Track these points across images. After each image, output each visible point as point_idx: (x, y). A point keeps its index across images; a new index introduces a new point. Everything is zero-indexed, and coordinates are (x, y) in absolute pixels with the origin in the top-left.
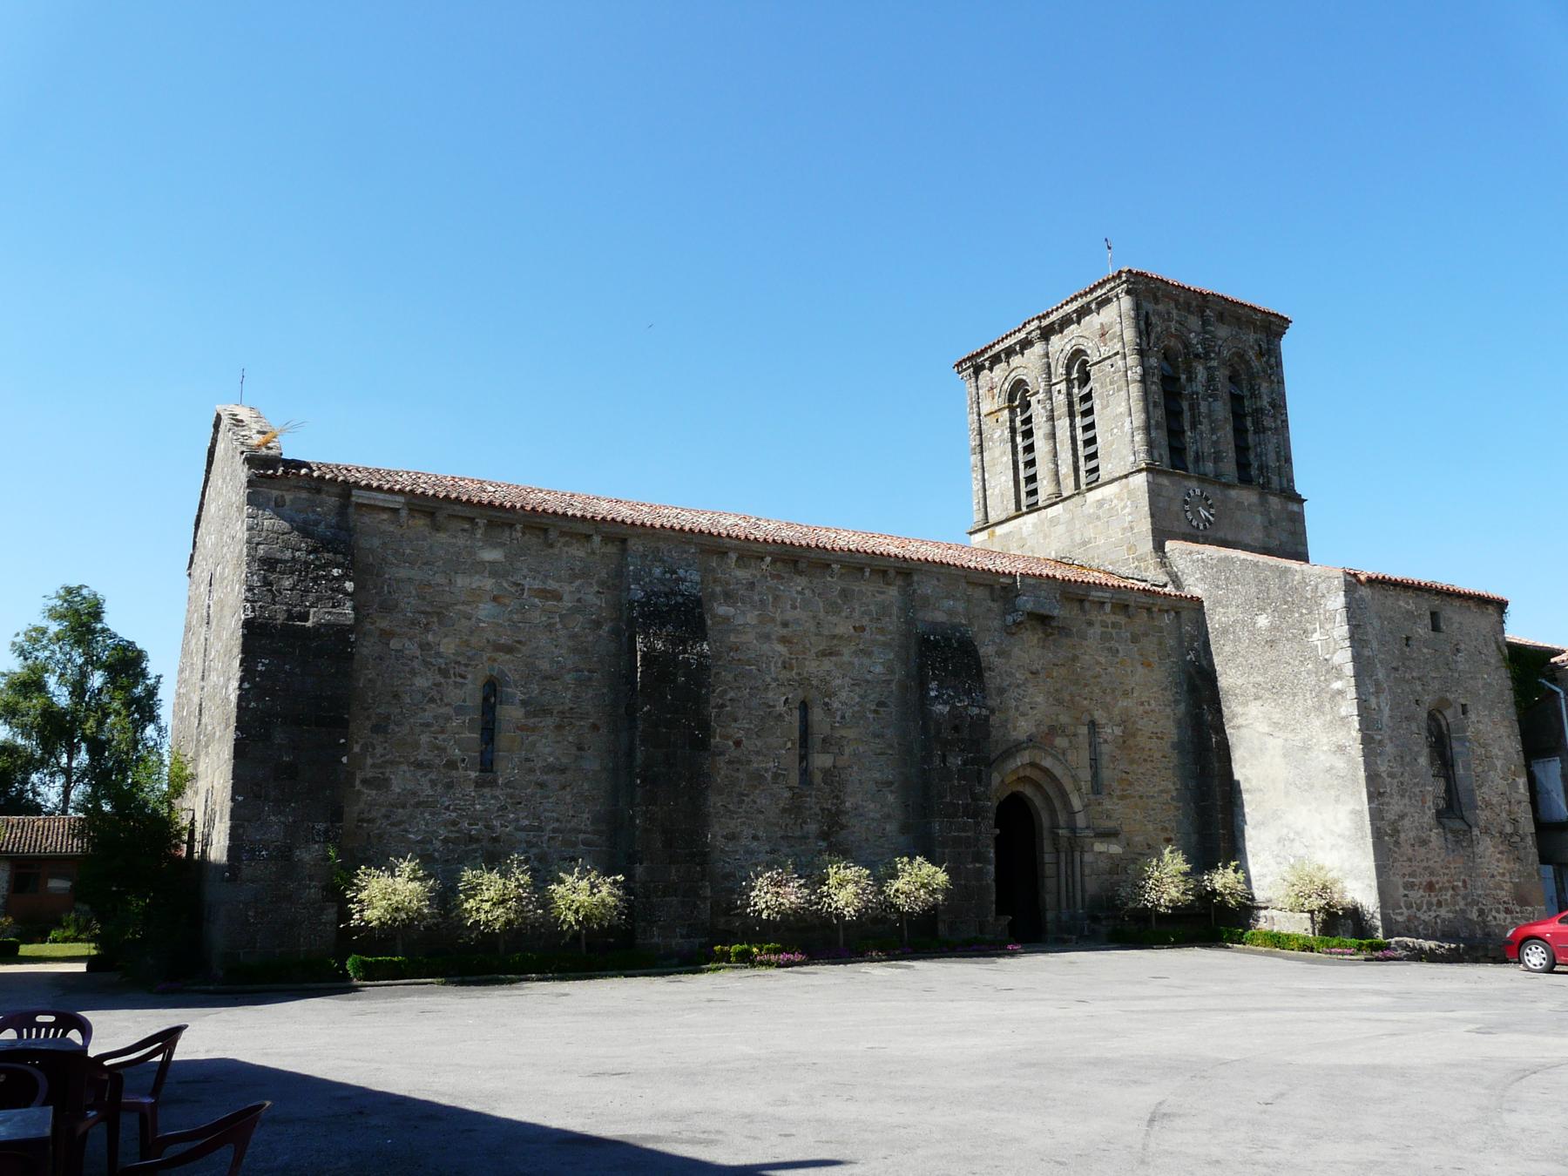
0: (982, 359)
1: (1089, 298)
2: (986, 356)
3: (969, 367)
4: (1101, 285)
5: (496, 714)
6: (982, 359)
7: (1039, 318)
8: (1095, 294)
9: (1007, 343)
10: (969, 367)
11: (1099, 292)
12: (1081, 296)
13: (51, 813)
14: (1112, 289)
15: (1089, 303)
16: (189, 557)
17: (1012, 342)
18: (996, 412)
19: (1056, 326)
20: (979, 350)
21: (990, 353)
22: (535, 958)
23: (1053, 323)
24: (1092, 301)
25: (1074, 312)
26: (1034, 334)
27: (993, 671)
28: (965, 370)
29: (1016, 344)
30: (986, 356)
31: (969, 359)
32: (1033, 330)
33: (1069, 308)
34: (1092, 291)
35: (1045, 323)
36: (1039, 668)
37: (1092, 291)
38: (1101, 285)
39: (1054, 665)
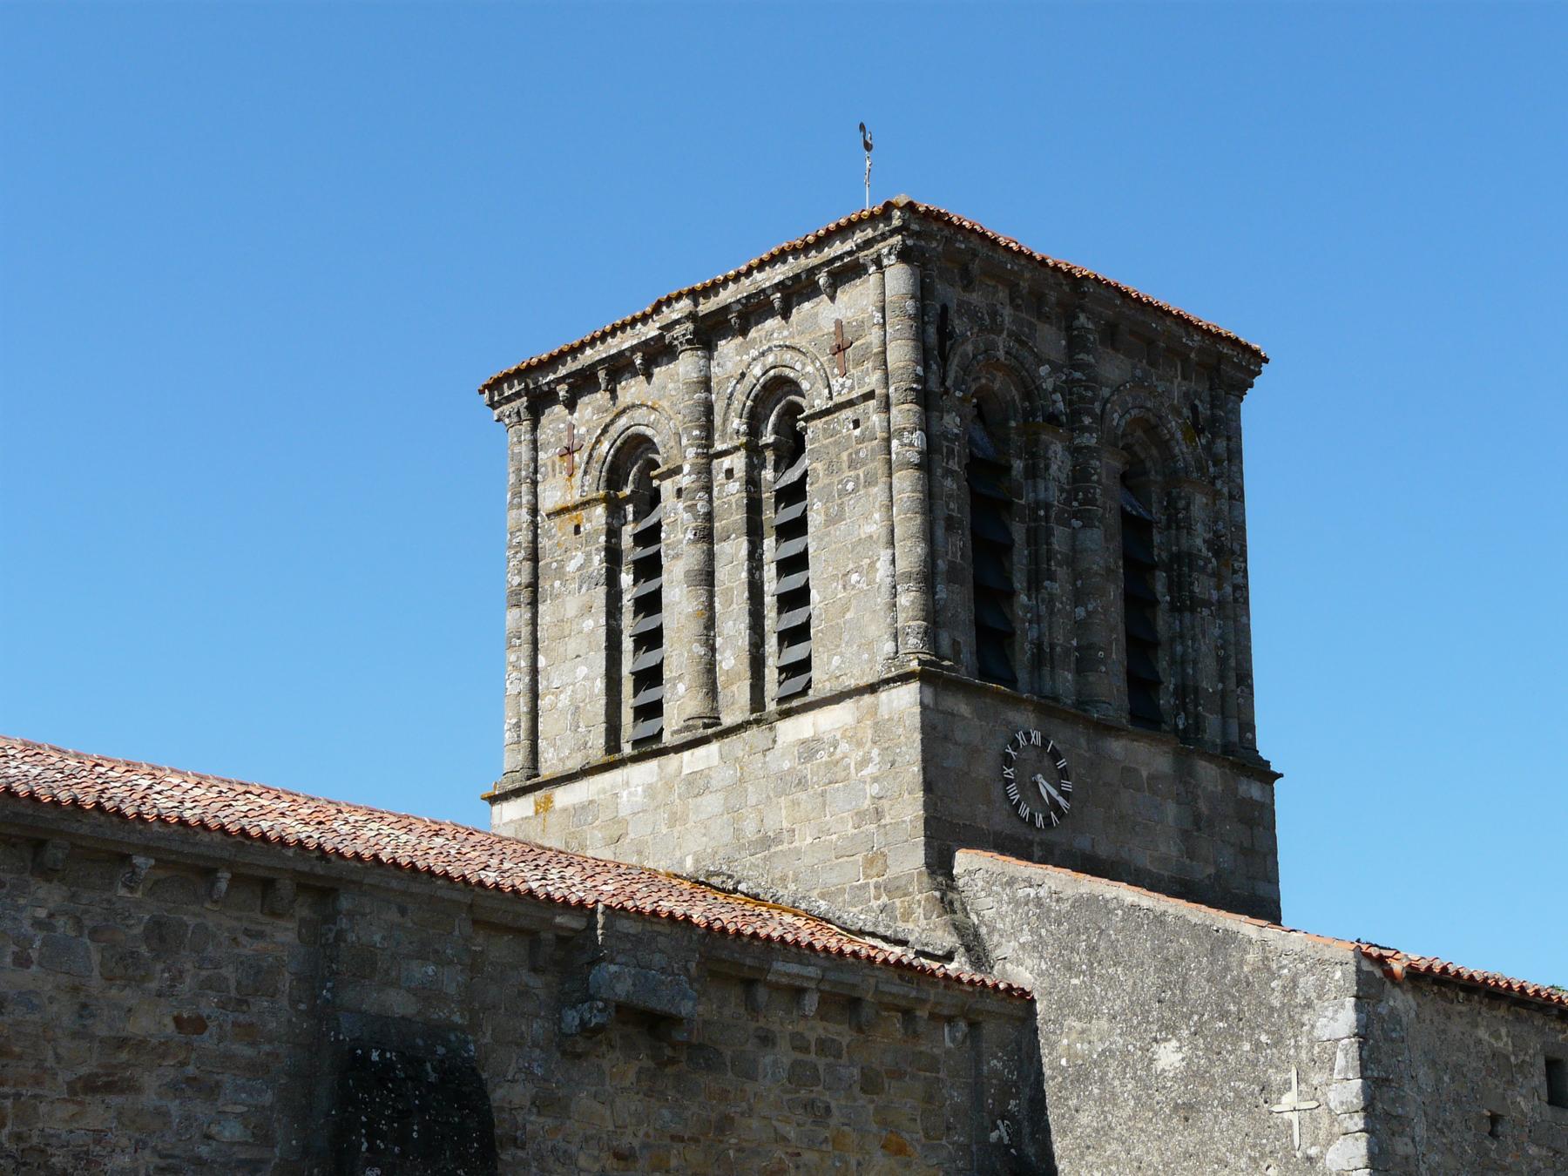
0: (551, 377)
1: (814, 258)
3: (518, 395)
6: (551, 377)
7: (694, 294)
8: (829, 253)
10: (518, 395)
11: (838, 248)
12: (795, 251)
14: (868, 244)
15: (812, 271)
21: (571, 366)
23: (726, 309)
26: (678, 331)
27: (523, 1148)
29: (633, 349)
30: (562, 371)
31: (520, 374)
32: (677, 322)
36: (636, 1144)
39: (673, 1138)
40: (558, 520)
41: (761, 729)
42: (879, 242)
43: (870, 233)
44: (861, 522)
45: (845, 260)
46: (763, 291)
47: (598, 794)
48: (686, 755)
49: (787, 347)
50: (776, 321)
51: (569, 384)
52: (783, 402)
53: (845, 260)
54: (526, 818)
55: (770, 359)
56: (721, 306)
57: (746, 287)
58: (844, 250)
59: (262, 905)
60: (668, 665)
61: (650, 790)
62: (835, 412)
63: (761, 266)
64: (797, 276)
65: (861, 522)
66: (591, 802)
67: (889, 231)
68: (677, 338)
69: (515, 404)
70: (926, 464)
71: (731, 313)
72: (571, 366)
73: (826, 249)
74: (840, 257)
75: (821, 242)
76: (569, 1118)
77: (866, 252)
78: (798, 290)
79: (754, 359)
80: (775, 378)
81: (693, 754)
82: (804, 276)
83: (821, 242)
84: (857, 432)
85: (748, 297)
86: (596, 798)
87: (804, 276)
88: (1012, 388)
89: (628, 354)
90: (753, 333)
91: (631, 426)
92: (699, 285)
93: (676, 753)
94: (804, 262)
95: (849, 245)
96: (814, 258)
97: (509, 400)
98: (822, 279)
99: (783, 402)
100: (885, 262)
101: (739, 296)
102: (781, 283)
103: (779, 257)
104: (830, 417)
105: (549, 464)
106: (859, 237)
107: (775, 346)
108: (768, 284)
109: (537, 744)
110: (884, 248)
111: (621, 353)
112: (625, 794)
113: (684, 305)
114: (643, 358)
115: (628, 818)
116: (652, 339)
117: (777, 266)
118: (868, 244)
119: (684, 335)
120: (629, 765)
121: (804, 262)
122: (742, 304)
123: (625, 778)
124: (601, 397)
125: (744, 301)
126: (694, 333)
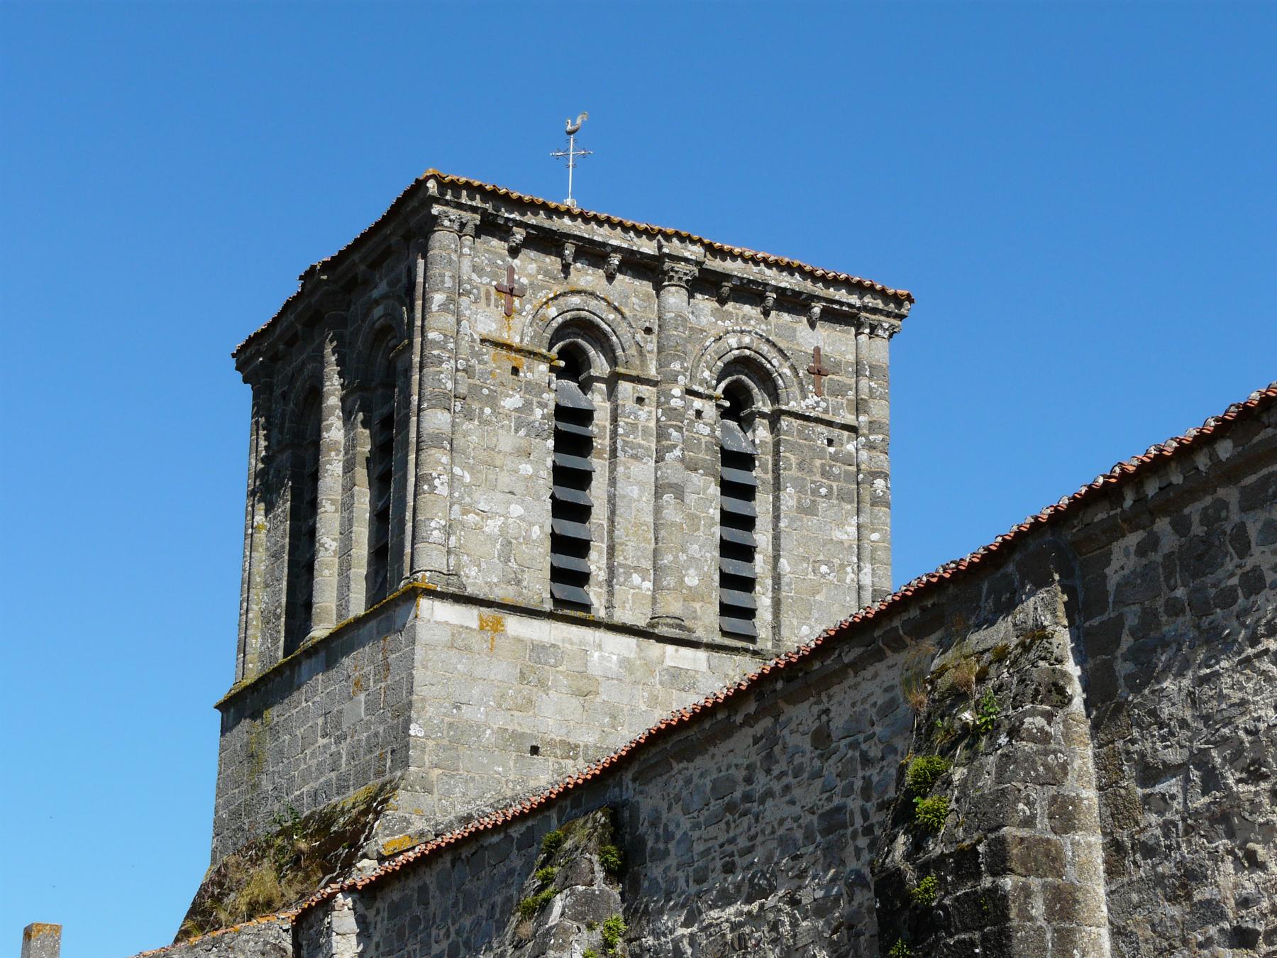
0: (516, 216)
1: (819, 289)
3: (474, 209)
6: (516, 216)
7: (709, 248)
8: (831, 292)
10: (474, 209)
11: (842, 295)
14: (874, 311)
15: (814, 298)
21: (540, 219)
23: (727, 277)
26: (681, 267)
29: (617, 249)
30: (530, 219)
32: (686, 260)
40: (492, 350)
41: (754, 660)
42: (883, 315)
43: (880, 304)
44: (833, 525)
45: (844, 308)
46: (766, 285)
47: (563, 641)
48: (670, 649)
49: (768, 340)
50: (754, 311)
51: (528, 233)
52: (735, 377)
53: (844, 308)
54: (467, 628)
55: (747, 340)
56: (723, 271)
57: (752, 272)
58: (849, 301)
61: (625, 662)
62: (811, 421)
63: (776, 265)
64: (800, 293)
65: (833, 525)
66: (553, 646)
67: (896, 314)
68: (677, 272)
69: (467, 216)
71: (728, 282)
72: (540, 219)
73: (832, 290)
74: (841, 304)
75: (835, 282)
77: (868, 315)
78: (794, 303)
79: (734, 331)
80: (747, 358)
81: (677, 651)
82: (804, 296)
83: (835, 282)
84: (832, 450)
85: (750, 281)
86: (560, 644)
87: (804, 296)
89: (609, 249)
90: (730, 306)
91: (583, 310)
92: (718, 244)
93: (657, 641)
94: (808, 286)
95: (854, 300)
96: (819, 289)
97: (460, 206)
99: (735, 377)
100: (880, 332)
101: (745, 276)
102: (785, 289)
103: (789, 269)
104: (805, 423)
105: (483, 290)
106: (868, 300)
107: (756, 333)
108: (773, 283)
109: (830, 644)
110: (886, 322)
111: (604, 245)
112: (596, 655)
113: (695, 252)
114: (621, 262)
115: (600, 679)
116: (642, 253)
117: (784, 274)
118: (874, 311)
119: (686, 274)
120: (602, 630)
121: (808, 286)
122: (741, 282)
123: (597, 640)
124: (552, 262)
125: (745, 281)
126: (695, 278)
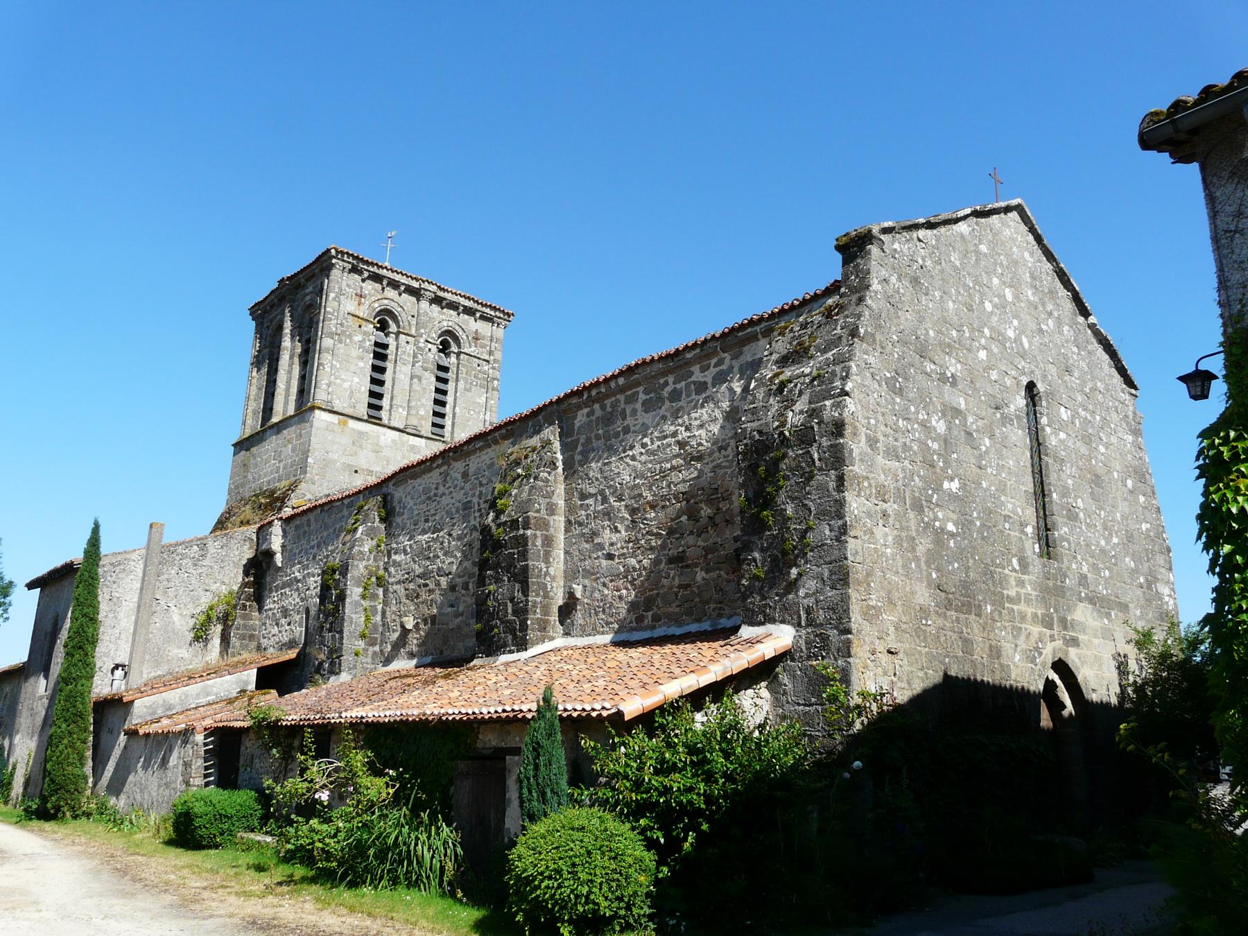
0: (365, 267)
1: (479, 307)
2: (371, 269)
3: (349, 263)
4: (494, 309)
5: (635, 632)
6: (365, 267)
7: (439, 287)
8: (484, 309)
9: (397, 277)
10: (349, 263)
11: (488, 310)
12: (477, 302)
13: (710, 455)
14: (499, 318)
15: (477, 310)
16: (59, 563)
17: (403, 281)
18: (362, 319)
19: (445, 302)
20: (365, 259)
21: (375, 269)
22: (1228, 769)
23: (445, 299)
24: (479, 311)
25: (463, 306)
26: (427, 293)
28: (343, 261)
29: (403, 284)
30: (371, 269)
31: (356, 258)
32: (430, 291)
33: (404, 280)
34: (486, 305)
35: (441, 294)
37: (486, 305)
38: (494, 309)
55: (450, 324)
59: (145, 745)
60: (207, 855)
69: (346, 265)
70: (343, 619)
76: (648, 895)
78: (469, 311)
88: (142, 760)
90: (445, 310)
94: (475, 306)
98: (478, 315)
106: (497, 313)
113: (433, 288)
